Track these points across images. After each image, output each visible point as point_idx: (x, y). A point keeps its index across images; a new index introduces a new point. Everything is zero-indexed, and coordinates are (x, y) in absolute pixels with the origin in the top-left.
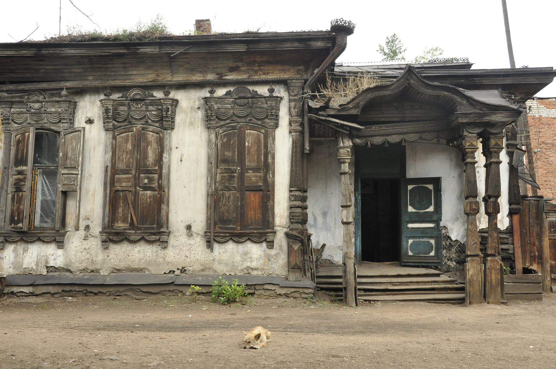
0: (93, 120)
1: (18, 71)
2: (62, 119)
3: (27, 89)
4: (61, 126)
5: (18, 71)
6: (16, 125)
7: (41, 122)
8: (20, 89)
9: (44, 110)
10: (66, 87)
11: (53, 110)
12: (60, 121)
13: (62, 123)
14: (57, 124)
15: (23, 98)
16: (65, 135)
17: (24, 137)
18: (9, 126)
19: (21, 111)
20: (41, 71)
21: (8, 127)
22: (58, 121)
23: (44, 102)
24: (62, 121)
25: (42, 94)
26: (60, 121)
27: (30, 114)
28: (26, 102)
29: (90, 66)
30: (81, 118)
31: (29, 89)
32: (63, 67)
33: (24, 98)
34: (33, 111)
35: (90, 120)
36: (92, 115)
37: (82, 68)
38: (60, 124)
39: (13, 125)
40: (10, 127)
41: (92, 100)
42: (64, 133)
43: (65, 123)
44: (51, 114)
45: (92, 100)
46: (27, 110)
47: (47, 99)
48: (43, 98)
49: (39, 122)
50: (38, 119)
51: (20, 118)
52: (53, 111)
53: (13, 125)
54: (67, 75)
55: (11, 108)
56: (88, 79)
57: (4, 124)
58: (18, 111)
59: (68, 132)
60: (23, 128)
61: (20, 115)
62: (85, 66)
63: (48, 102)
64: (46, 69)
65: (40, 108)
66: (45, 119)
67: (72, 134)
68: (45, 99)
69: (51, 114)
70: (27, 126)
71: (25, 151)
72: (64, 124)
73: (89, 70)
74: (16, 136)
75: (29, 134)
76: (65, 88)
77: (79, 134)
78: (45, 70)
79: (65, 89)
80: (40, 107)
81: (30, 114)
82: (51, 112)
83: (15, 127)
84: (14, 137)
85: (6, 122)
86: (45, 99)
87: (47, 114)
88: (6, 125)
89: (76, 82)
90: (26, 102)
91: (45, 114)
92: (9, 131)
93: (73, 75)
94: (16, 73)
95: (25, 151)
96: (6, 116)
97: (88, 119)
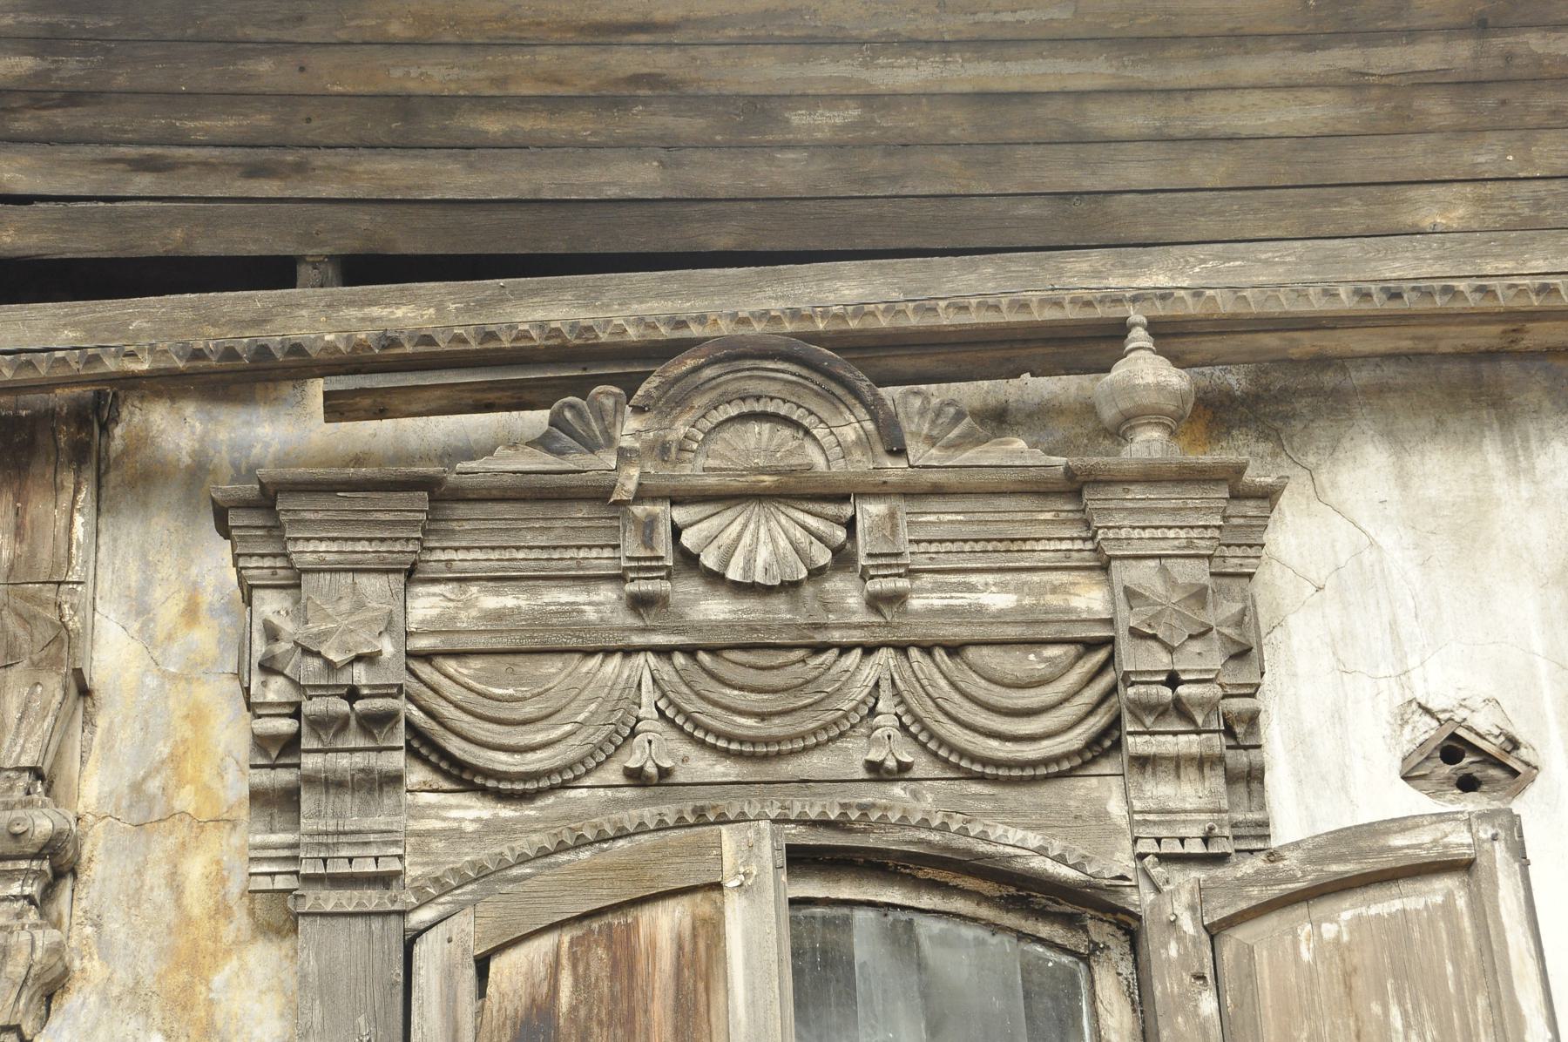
0: (1514, 744)
1: (493, 125)
2: (1142, 708)
3: (633, 334)
4: (1116, 808)
5: (493, 125)
6: (471, 811)
7: (817, 764)
8: (538, 339)
9: (875, 602)
10: (1160, 310)
11: (997, 599)
12: (1105, 744)
13: (1143, 763)
14: (1048, 794)
15: (591, 446)
16: (1214, 932)
17: (625, 962)
18: (379, 821)
19: (539, 620)
20: (798, 118)
21: (358, 837)
22: (1075, 739)
23: (879, 492)
24: (1137, 744)
25: (847, 392)
26: (1105, 744)
27: (664, 652)
28: (642, 496)
29: (1461, 53)
30: (1338, 717)
31: (665, 332)
32: (1097, 71)
33: (610, 441)
34: (716, 608)
35: (1452, 748)
36: (1480, 687)
37: (1356, 84)
38: (1084, 788)
39: (420, 812)
40: (389, 837)
41: (1433, 491)
42: (1203, 893)
43: (1177, 764)
44: (955, 649)
45: (1433, 491)
46: (639, 603)
47: (918, 452)
48: (864, 443)
49: (789, 768)
50: (776, 727)
51: (529, 710)
52: (1000, 617)
53: (420, 812)
54: (1139, 174)
55: (412, 575)
56: (1407, 219)
57: (307, 801)
58: (499, 615)
59: (1255, 879)
60: (581, 843)
61: (525, 665)
62: (1389, 58)
63: (938, 492)
64: (870, 99)
65: (816, 573)
66: (886, 721)
67: (1344, 915)
68: (899, 452)
69: (955, 649)
70: (630, 818)
71: (1456, 1022)
72: (1161, 790)
73: (1437, 108)
74: (482, 966)
75: (710, 931)
76: (1136, 315)
77: (1448, 907)
78: (854, 113)
79: (1139, 337)
80: (823, 557)
81: (664, 652)
82: (963, 633)
83: (455, 836)
84: (449, 975)
85: (344, 762)
86: (899, 452)
87: (902, 648)
88: (330, 802)
89: (1266, 251)
90: (642, 496)
91: (885, 655)
92: (372, 898)
93: (1207, 169)
94: (469, 147)
95: (1456, 1022)
96: (360, 675)
97: (1425, 729)
